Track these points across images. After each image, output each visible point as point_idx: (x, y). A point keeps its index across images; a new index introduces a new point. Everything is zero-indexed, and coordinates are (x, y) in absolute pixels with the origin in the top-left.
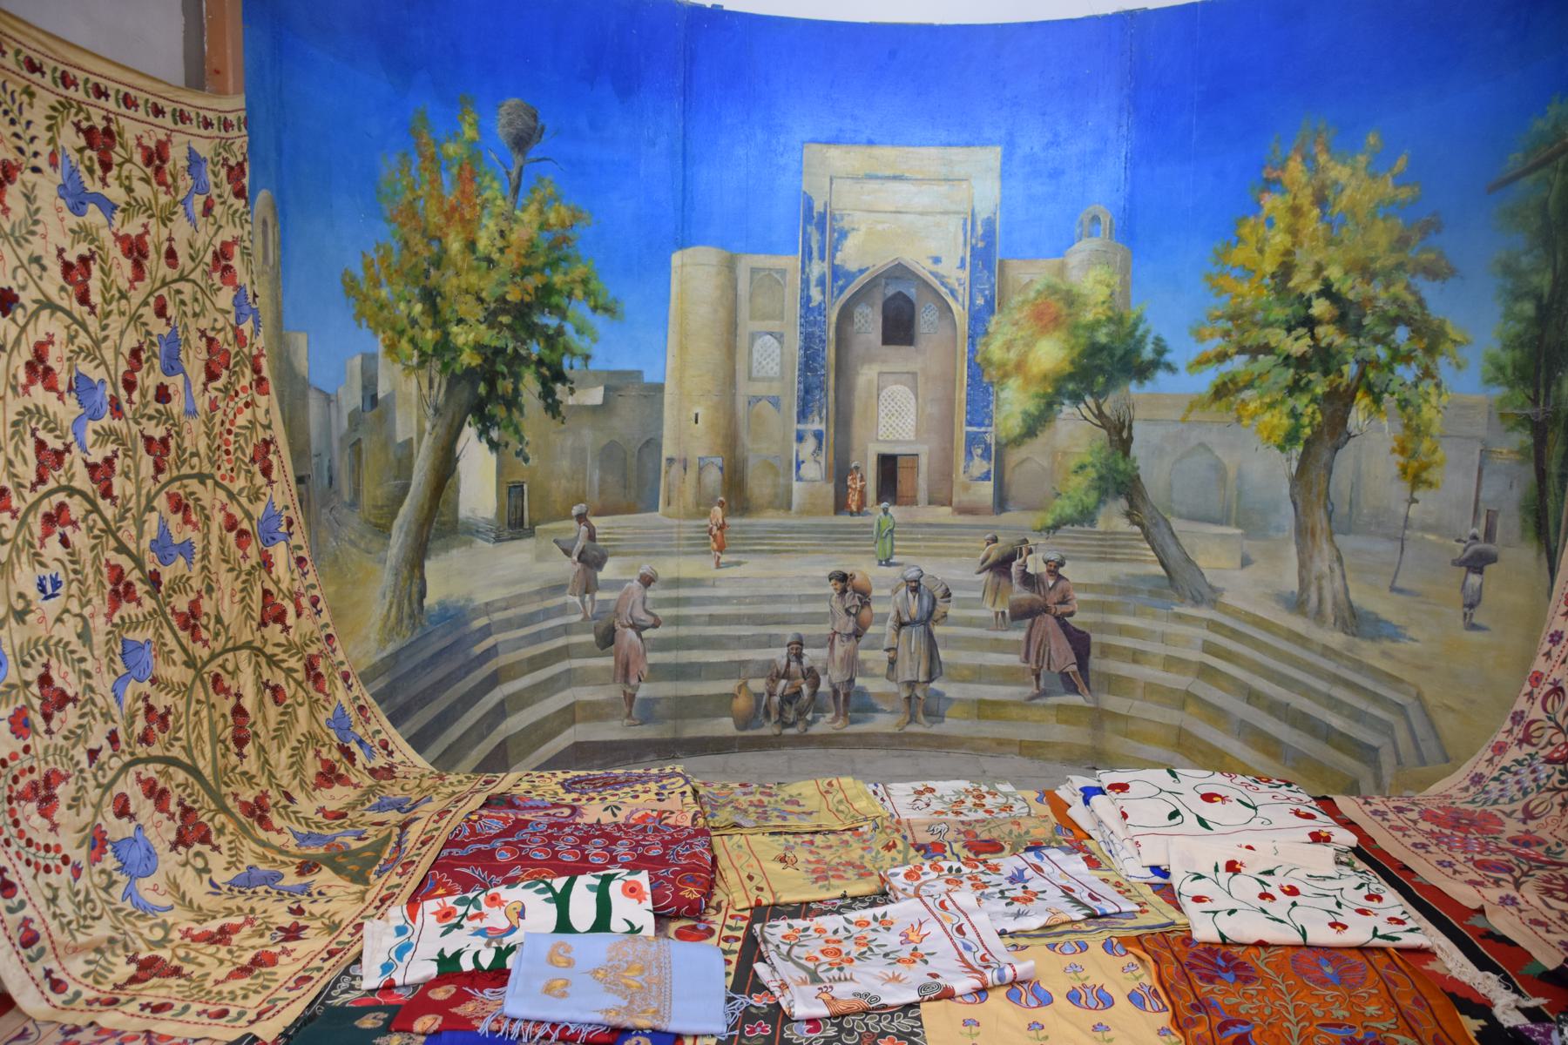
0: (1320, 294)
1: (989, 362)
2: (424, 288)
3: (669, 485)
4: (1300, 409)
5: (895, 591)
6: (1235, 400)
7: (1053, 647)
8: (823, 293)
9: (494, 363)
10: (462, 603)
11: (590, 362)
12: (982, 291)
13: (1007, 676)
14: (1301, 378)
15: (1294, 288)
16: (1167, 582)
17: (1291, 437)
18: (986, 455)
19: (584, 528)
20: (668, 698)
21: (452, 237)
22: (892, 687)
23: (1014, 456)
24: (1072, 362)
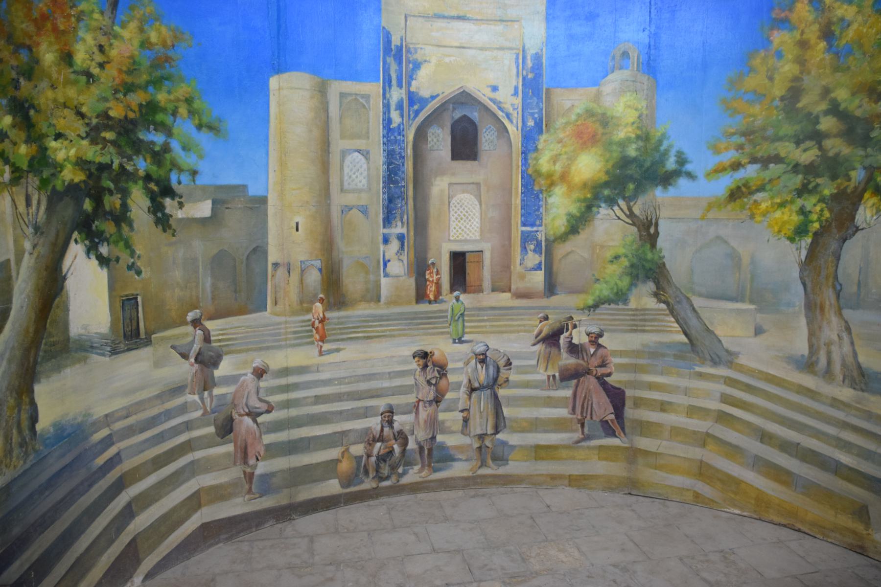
0: (827, 113)
1: (538, 173)
2: (14, 99)
3: (275, 287)
4: (809, 207)
5: (467, 363)
6: (748, 201)
7: (595, 400)
8: (402, 116)
9: (99, 178)
10: (80, 420)
11: (197, 177)
12: (532, 114)
13: (558, 425)
14: (809, 182)
15: (802, 108)
16: (689, 347)
17: (801, 231)
18: (537, 250)
19: (199, 332)
20: (282, 471)
21: (43, 47)
22: (467, 440)
23: (560, 250)
24: (607, 172)
